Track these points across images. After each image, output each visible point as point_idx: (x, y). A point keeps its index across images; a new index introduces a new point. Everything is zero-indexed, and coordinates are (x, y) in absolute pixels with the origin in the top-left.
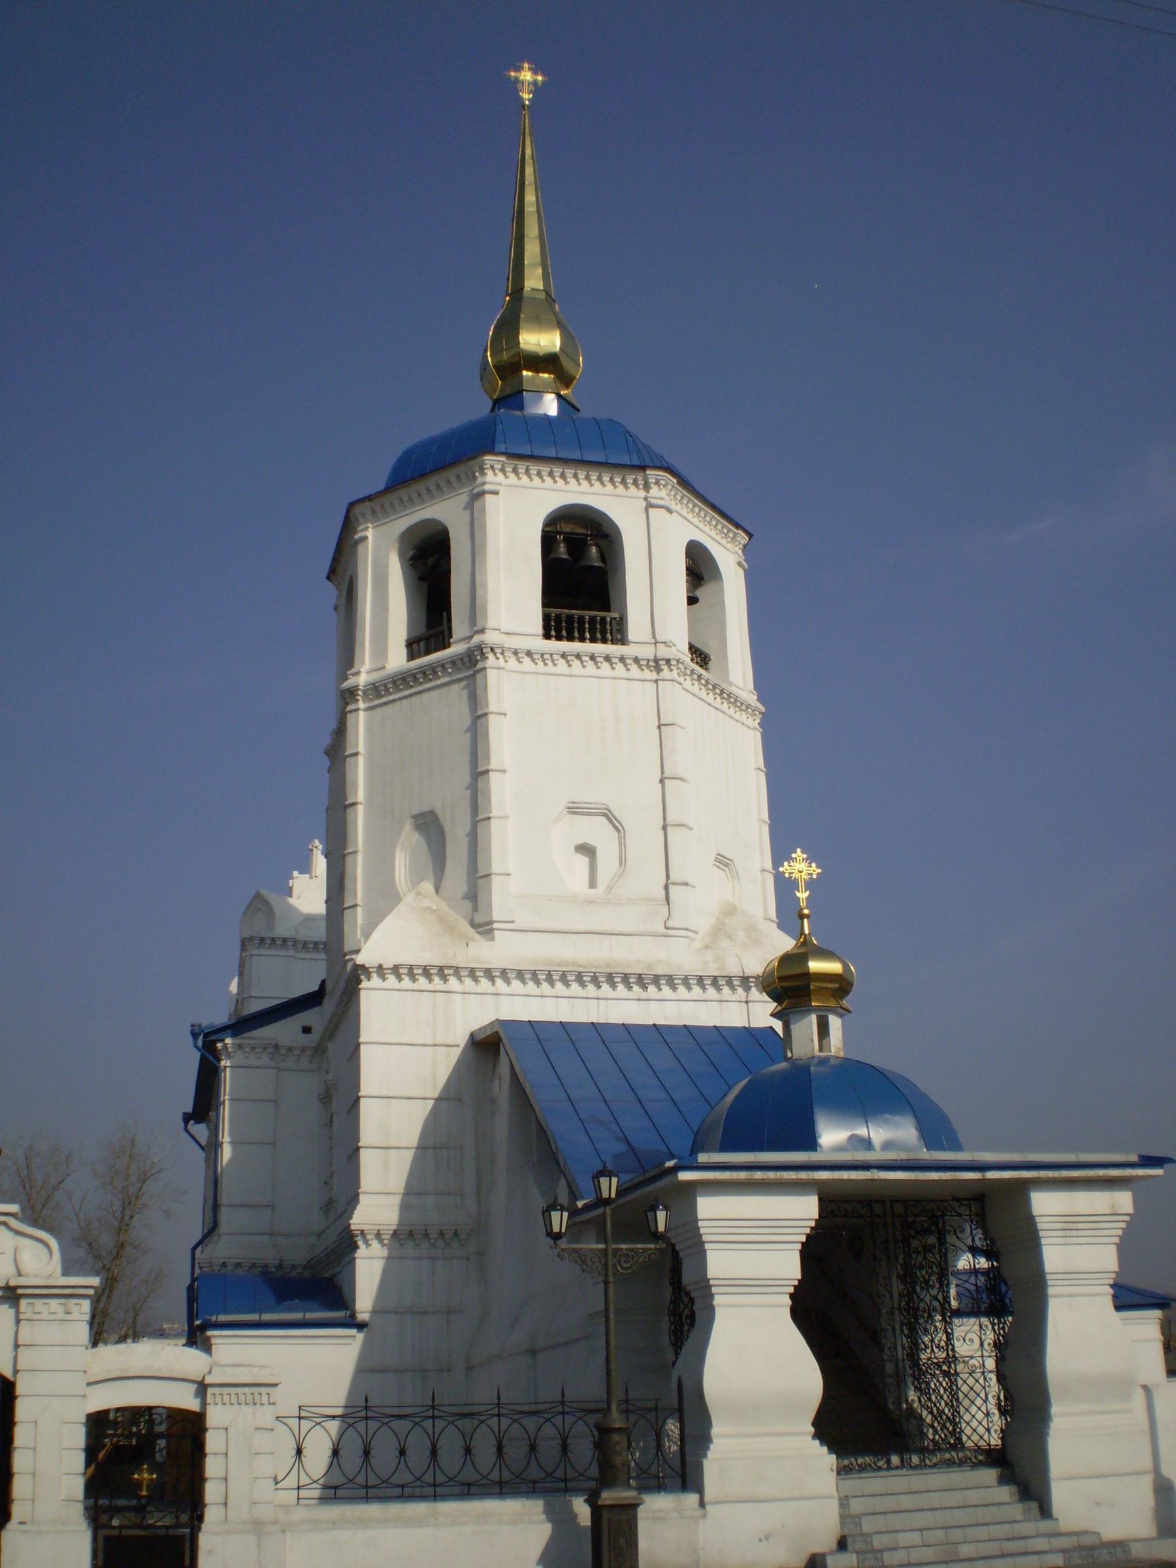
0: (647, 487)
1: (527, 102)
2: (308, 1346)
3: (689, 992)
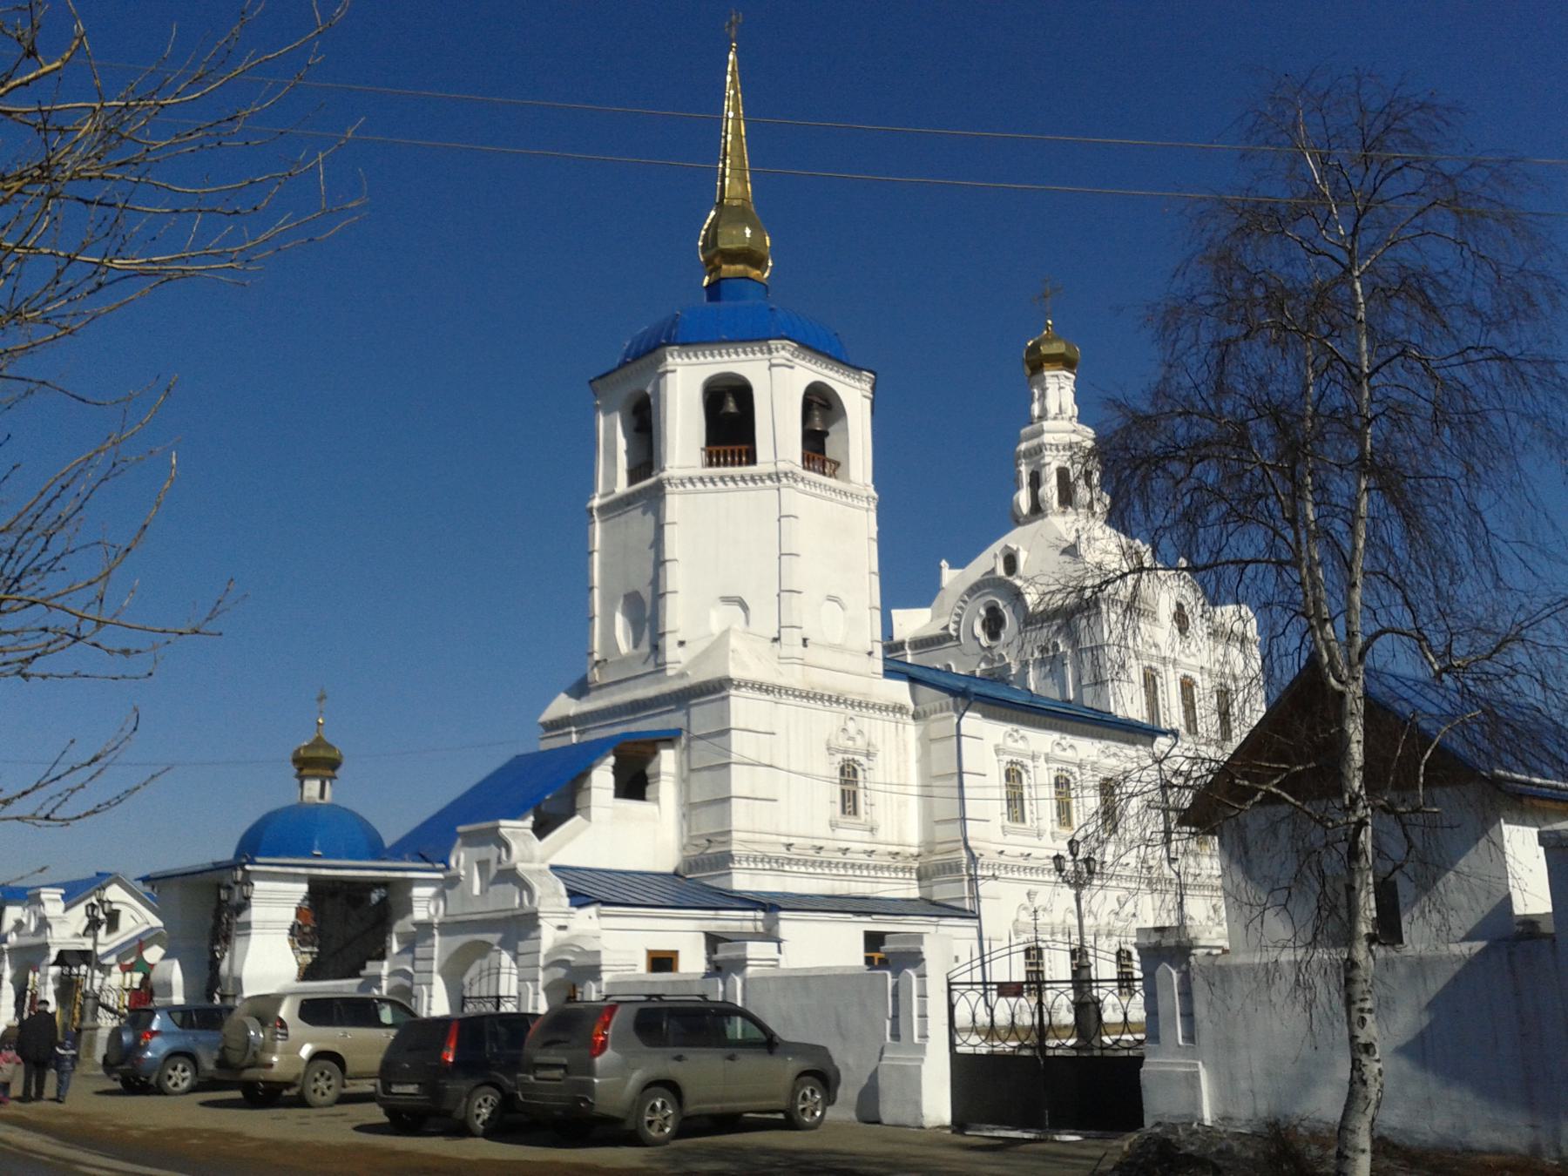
0: (770, 351)
2: (628, 992)
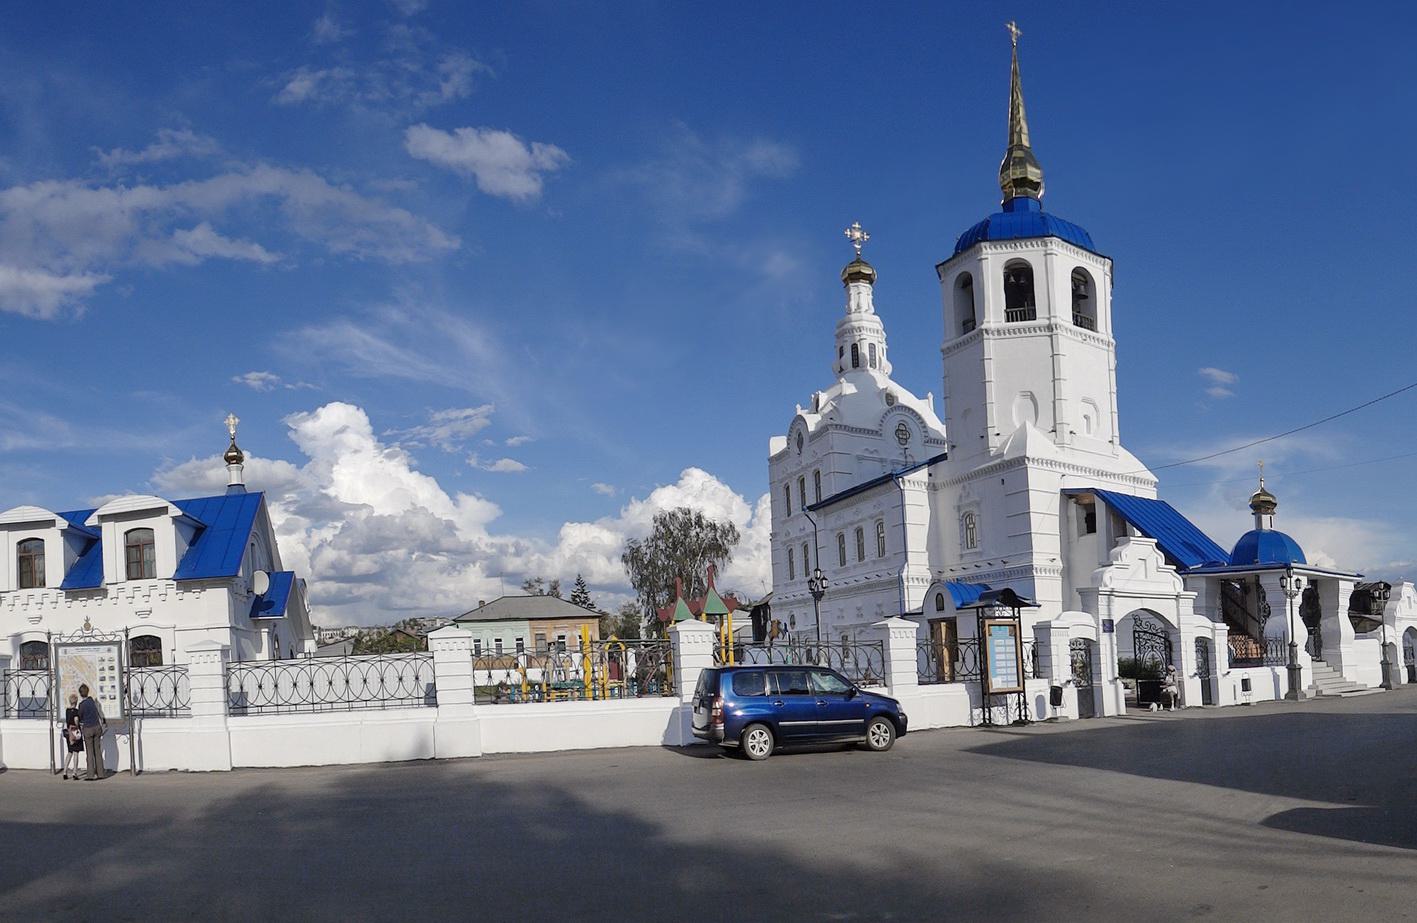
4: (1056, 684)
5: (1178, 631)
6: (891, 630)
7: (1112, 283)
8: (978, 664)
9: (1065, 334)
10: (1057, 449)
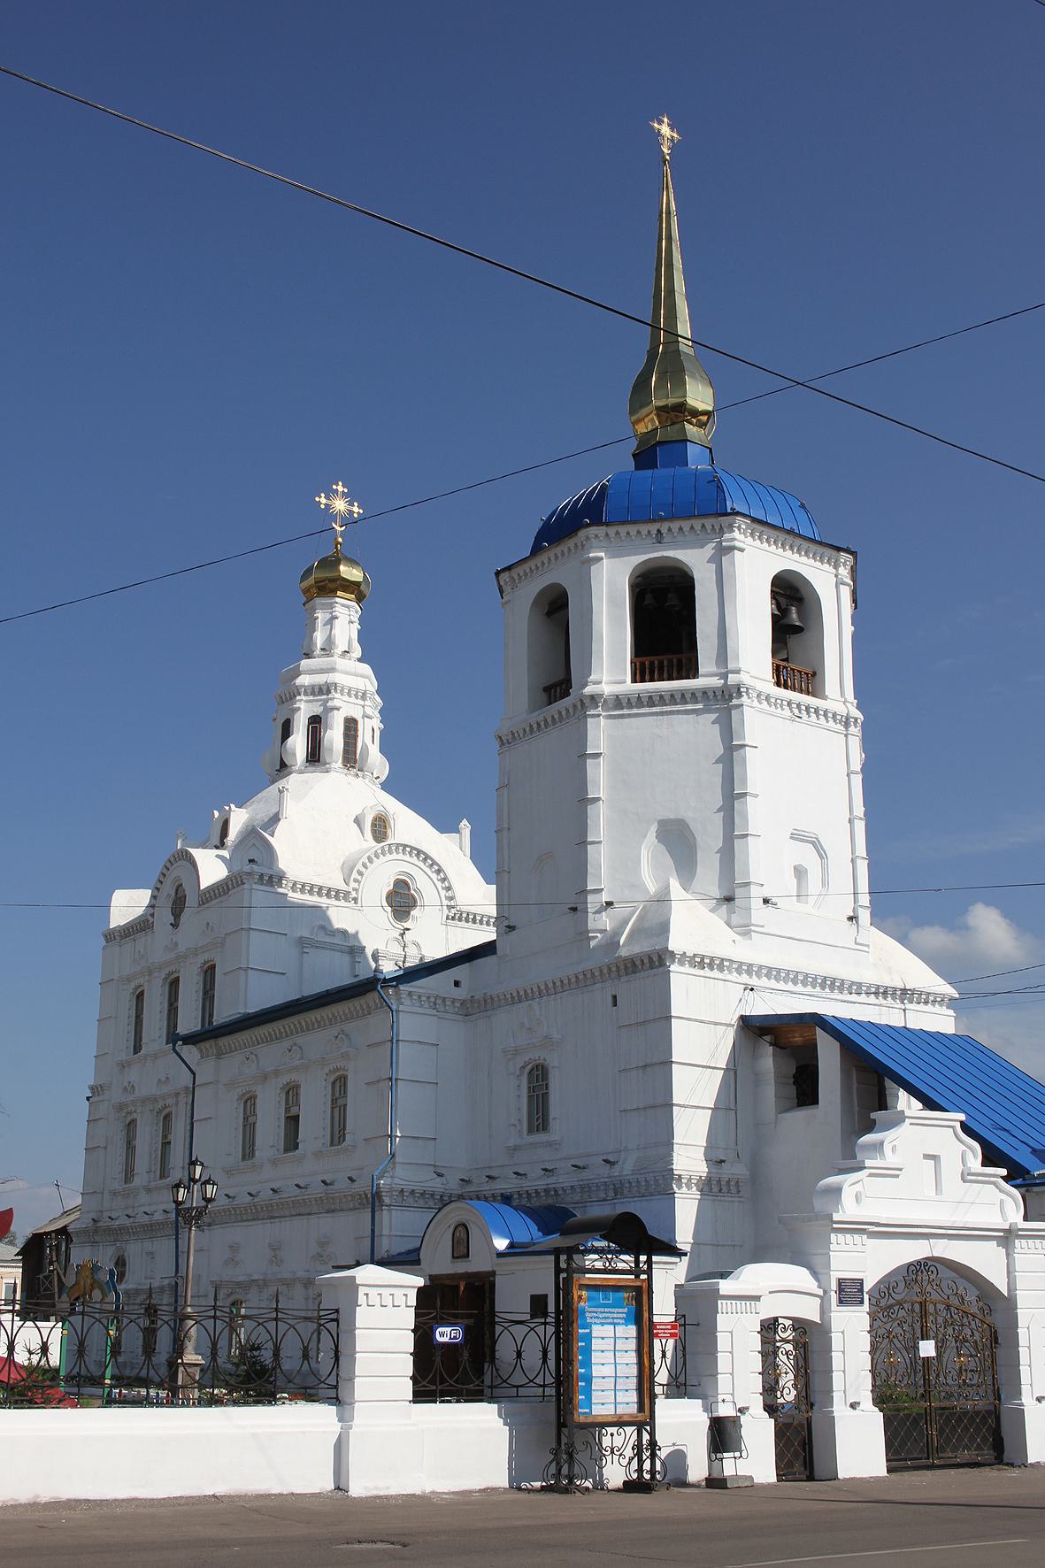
1: (668, 157)
3: (357, 933)
4: (725, 1411)
5: (1009, 1304)
6: (362, 1291)
7: (855, 601)
8: (552, 1363)
9: (756, 703)
10: (737, 938)
